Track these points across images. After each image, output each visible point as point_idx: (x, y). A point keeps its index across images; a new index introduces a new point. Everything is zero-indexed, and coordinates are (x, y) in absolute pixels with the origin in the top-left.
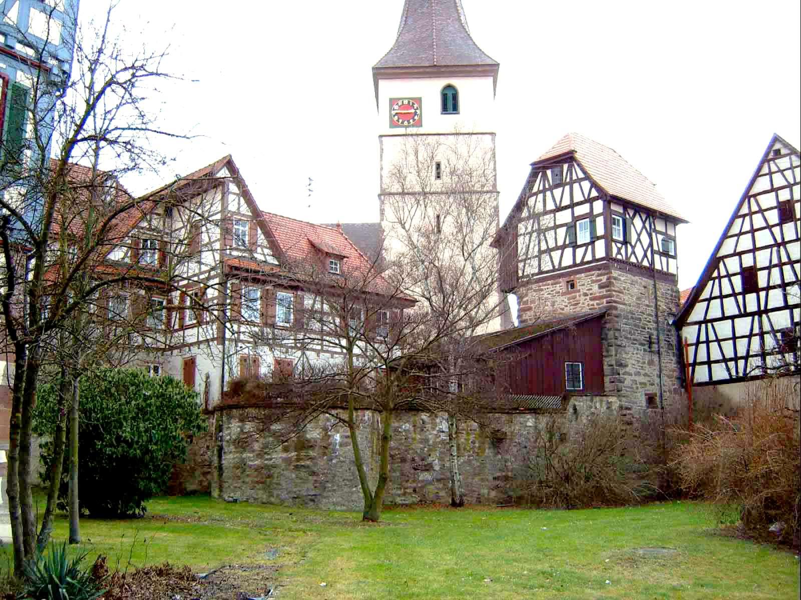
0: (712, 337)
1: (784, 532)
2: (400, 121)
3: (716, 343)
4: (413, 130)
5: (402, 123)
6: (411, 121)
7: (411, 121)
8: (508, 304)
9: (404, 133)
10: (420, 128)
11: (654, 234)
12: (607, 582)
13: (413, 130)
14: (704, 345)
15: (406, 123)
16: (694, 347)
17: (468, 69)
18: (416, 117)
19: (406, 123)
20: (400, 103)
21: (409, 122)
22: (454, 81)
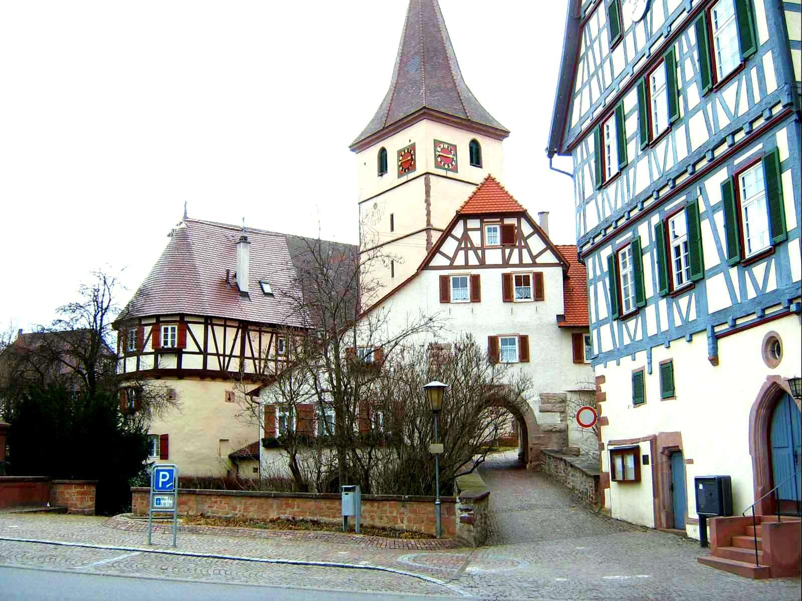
0: (257, 362)
1: (114, 379)
2: (443, 163)
3: (251, 361)
4: (450, 174)
5: (444, 165)
6: (450, 165)
7: (450, 165)
8: (778, 84)
9: (444, 174)
10: (456, 174)
11: (154, 321)
12: (120, 415)
13: (450, 174)
14: (238, 360)
15: (446, 166)
16: (123, 360)
17: (405, 121)
18: (453, 163)
19: (446, 166)
20: (442, 146)
21: (449, 166)
22: (480, 139)
